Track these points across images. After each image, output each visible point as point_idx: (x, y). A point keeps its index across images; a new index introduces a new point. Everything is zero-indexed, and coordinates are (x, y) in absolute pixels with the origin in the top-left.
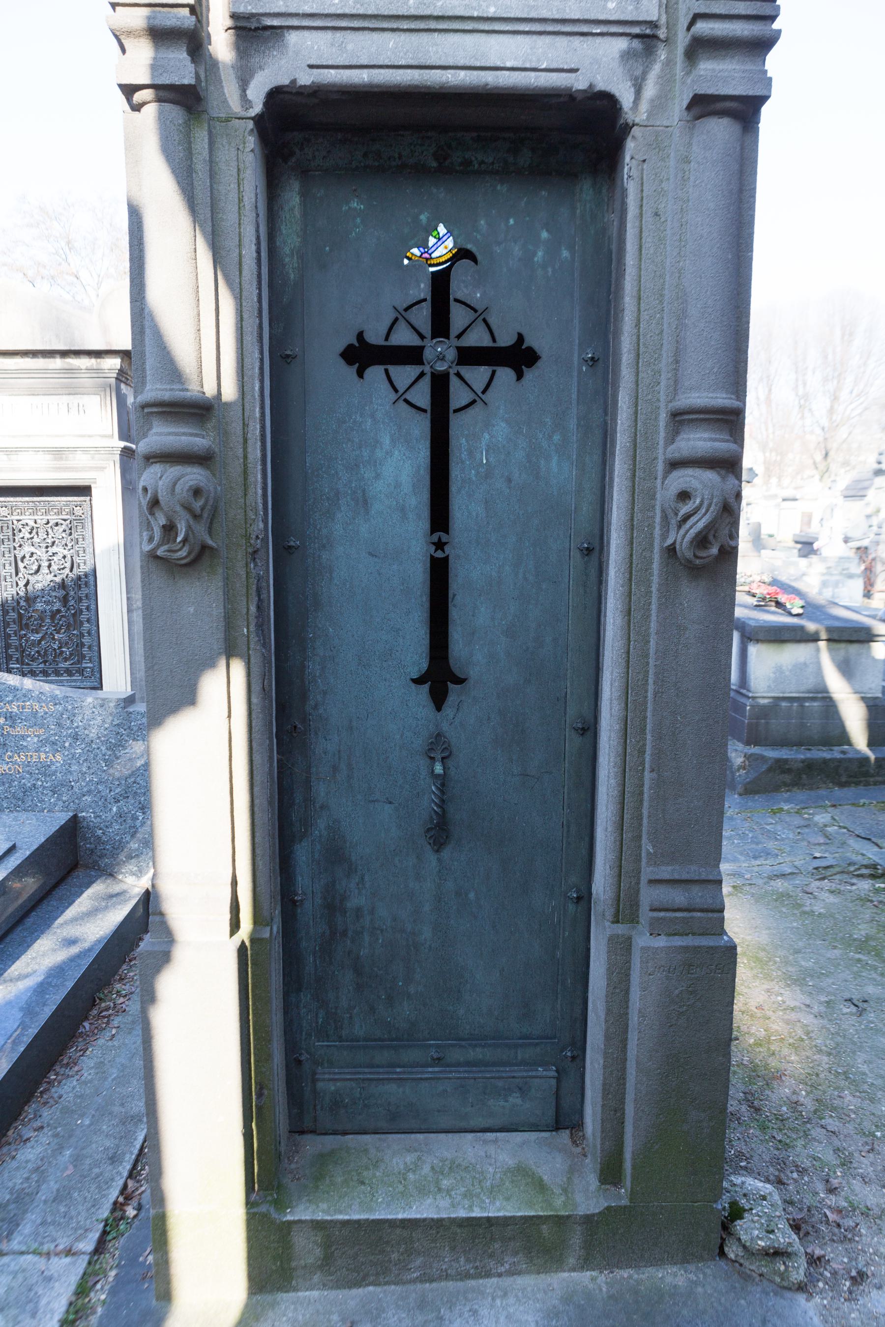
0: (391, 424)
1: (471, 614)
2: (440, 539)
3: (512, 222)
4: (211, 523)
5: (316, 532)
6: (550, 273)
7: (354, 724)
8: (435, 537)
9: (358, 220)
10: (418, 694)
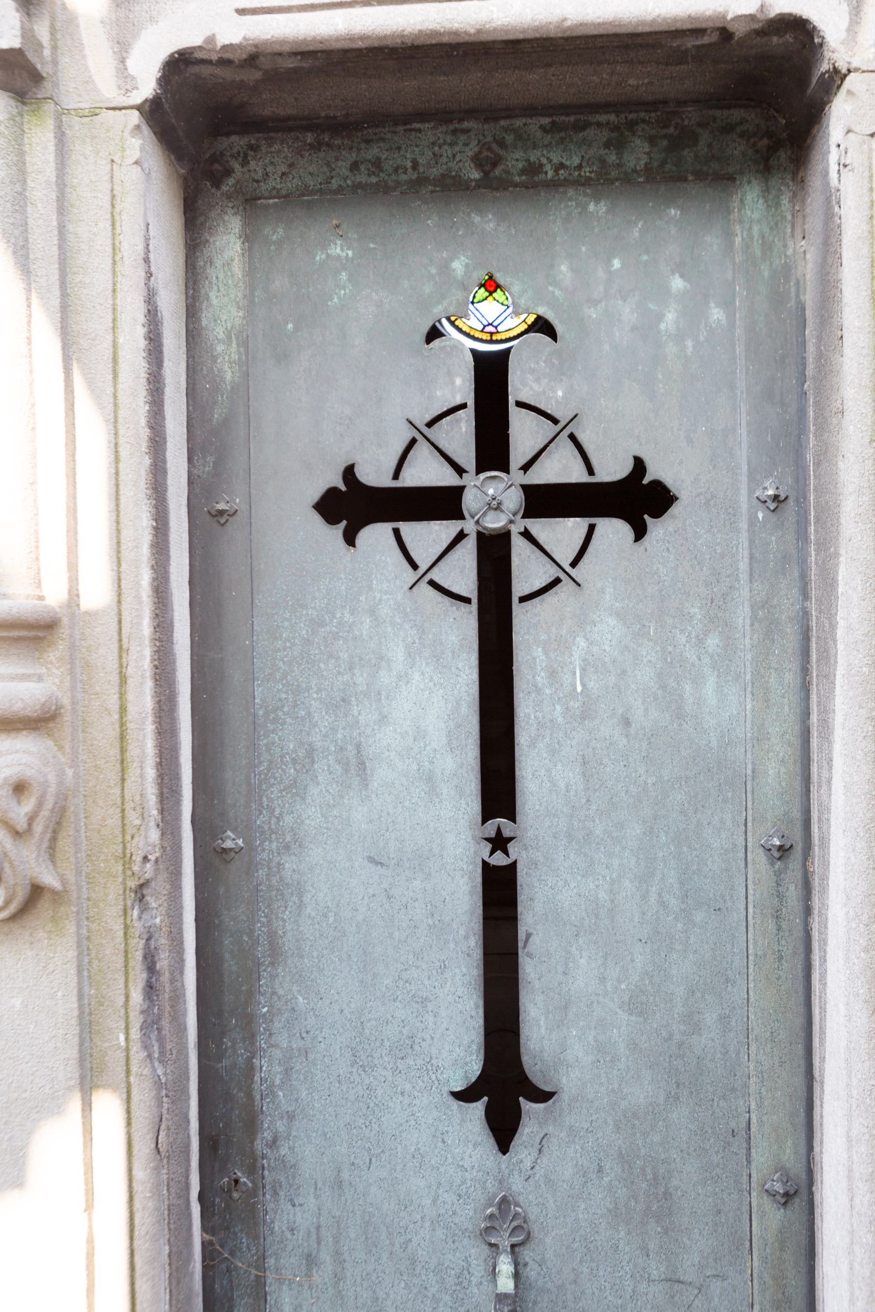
0: (407, 626)
1: (560, 969)
3: (617, 264)
4: (54, 839)
5: (274, 820)
6: (690, 350)
7: (345, 1175)
9: (344, 276)
10: (463, 1120)
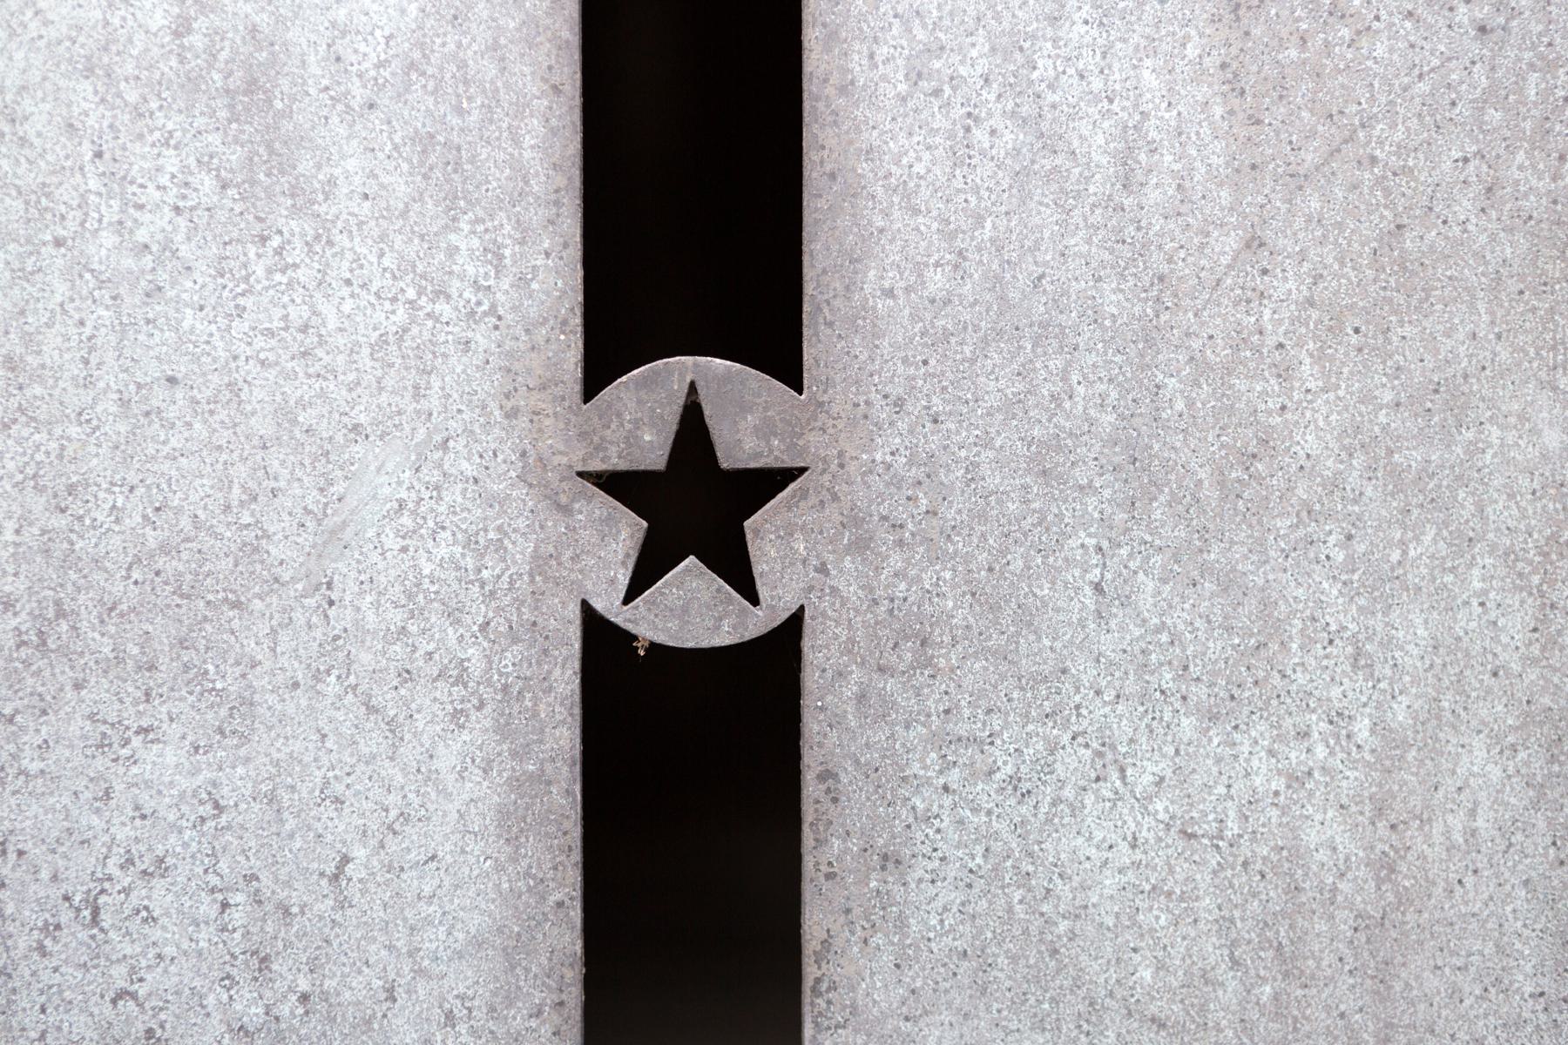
2: (693, 428)
8: (639, 417)
